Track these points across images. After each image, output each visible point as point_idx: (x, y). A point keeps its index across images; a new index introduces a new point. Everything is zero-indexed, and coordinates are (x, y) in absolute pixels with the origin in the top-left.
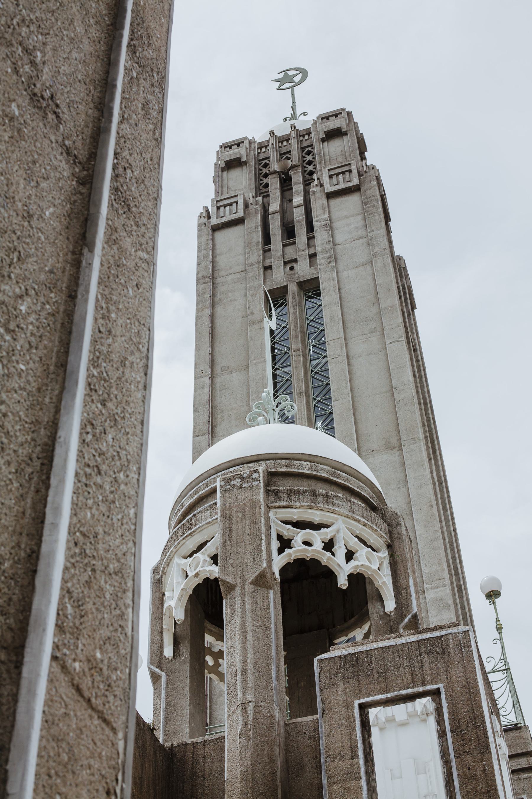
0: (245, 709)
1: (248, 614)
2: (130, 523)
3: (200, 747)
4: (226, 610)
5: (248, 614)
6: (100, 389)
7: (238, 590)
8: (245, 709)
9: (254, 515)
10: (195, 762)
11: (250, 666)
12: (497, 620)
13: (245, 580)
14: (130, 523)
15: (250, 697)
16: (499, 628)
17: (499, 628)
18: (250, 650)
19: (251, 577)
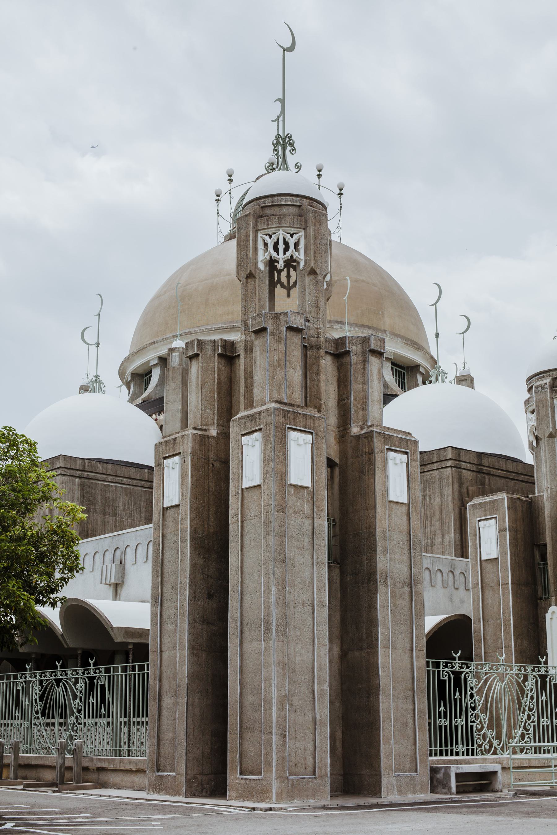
0: (547, 490)
1: (547, 451)
2: (299, 410)
3: (540, 497)
4: (187, 490)
5: (547, 451)
6: (305, 325)
7: (543, 440)
8: (547, 490)
9: (546, 406)
10: (538, 503)
11: (548, 473)
12: (218, 210)
13: (545, 436)
14: (299, 410)
15: (549, 486)
16: (341, 208)
17: (341, 208)
18: (548, 467)
19: (547, 435)
